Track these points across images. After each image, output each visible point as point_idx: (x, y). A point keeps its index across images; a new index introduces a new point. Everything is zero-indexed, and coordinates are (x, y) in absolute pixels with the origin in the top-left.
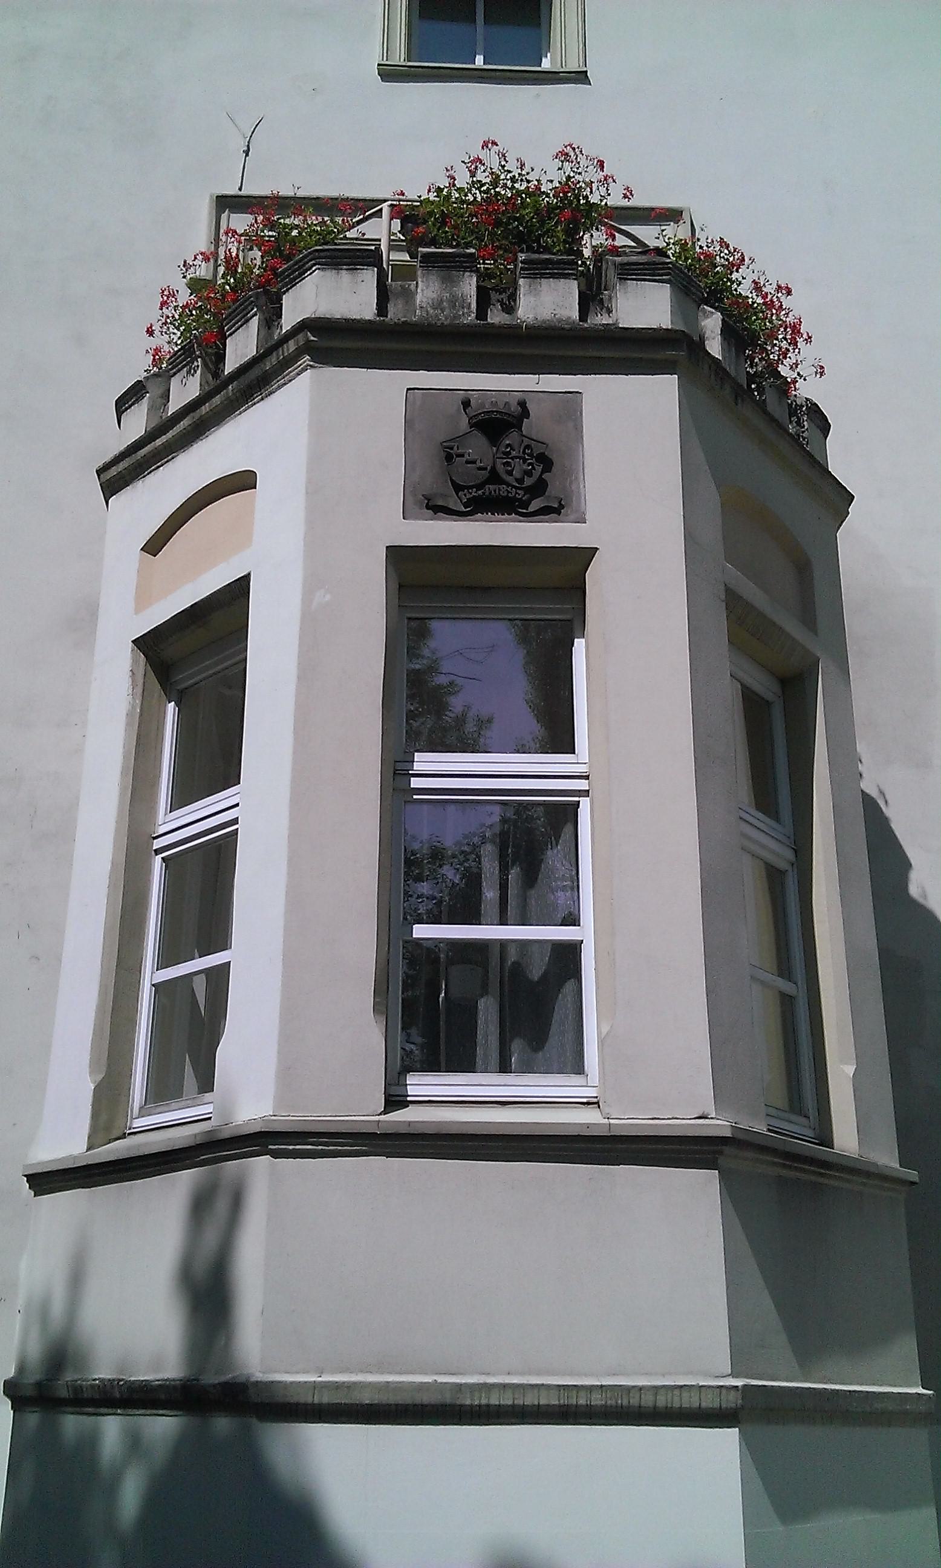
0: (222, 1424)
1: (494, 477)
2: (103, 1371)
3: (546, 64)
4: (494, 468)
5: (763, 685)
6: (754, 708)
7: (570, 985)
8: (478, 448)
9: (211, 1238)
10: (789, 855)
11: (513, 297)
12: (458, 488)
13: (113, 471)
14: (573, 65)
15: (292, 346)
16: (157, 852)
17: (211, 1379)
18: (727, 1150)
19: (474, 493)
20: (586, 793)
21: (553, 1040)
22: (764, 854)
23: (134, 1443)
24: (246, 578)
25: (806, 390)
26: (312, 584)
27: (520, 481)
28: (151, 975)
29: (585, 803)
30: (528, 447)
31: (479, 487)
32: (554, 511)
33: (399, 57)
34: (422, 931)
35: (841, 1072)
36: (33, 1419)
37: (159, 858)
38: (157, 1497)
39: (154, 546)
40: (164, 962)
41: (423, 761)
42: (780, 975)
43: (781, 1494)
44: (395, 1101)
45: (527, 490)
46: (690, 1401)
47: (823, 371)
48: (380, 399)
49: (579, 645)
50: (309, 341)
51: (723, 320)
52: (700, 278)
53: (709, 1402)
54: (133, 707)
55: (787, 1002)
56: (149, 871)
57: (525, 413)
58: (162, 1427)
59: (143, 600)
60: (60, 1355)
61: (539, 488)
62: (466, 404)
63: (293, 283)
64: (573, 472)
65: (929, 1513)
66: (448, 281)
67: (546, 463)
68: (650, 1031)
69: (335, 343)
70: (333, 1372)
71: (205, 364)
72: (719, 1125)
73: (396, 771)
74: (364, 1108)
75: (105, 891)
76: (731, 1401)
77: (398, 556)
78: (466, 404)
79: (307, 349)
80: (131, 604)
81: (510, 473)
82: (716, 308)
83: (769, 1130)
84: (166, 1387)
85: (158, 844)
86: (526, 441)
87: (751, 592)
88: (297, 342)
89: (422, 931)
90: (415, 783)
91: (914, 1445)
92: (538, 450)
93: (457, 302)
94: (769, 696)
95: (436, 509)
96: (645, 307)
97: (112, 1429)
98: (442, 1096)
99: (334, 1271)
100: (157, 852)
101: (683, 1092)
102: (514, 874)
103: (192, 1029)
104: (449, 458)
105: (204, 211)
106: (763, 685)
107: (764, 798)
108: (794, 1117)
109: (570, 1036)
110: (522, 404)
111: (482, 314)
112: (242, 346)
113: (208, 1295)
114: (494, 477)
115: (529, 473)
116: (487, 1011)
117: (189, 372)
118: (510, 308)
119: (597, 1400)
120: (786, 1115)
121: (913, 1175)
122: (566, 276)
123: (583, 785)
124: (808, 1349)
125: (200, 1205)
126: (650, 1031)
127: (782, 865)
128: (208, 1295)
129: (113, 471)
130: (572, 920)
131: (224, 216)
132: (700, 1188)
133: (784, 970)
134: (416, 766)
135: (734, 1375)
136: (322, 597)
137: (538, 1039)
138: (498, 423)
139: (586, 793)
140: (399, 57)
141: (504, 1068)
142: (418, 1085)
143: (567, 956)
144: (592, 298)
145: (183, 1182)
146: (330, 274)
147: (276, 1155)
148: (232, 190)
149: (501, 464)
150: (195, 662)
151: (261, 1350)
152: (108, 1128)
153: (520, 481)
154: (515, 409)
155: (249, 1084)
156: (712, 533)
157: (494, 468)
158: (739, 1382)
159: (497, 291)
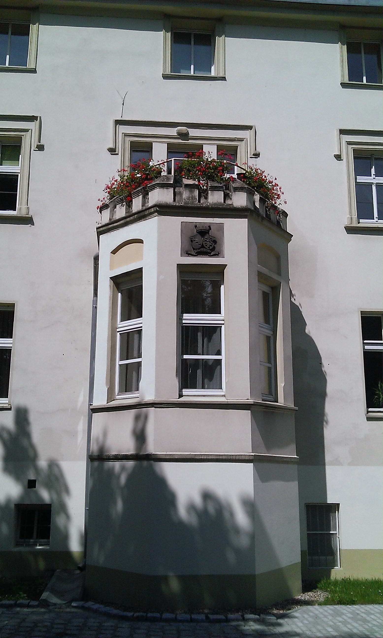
0: (145, 463)
1: (203, 246)
2: (114, 453)
3: (213, 74)
4: (203, 244)
5: (267, 289)
6: (265, 295)
7: (219, 367)
8: (199, 239)
9: (140, 425)
10: (272, 333)
11: (207, 194)
12: (194, 249)
13: (101, 229)
14: (221, 75)
15: (152, 210)
16: (118, 332)
17: (142, 453)
18: (253, 406)
19: (198, 250)
20: (224, 324)
21: (214, 379)
22: (265, 334)
23: (123, 468)
24: (142, 268)
25: (282, 207)
26: (159, 273)
27: (209, 248)
28: (118, 362)
29: (223, 326)
30: (211, 239)
31: (199, 249)
32: (217, 255)
33: (168, 72)
34: (185, 357)
35: (281, 385)
36: (96, 463)
37: (118, 333)
38: (130, 478)
39: (114, 252)
40: (121, 360)
41: (186, 316)
42: (268, 363)
43: (261, 477)
44: (181, 396)
45: (210, 250)
46: (243, 458)
47: (288, 201)
48: (175, 223)
49: (222, 286)
50: (157, 210)
51: (260, 197)
52: (255, 184)
53: (247, 458)
54: (111, 295)
55: (269, 369)
56: (116, 336)
57: (210, 229)
58: (130, 464)
59: (112, 267)
60: (102, 450)
61: (214, 249)
62: (196, 226)
63: (152, 190)
64: (222, 245)
65: (296, 483)
66: (191, 192)
67: (215, 242)
68: (237, 378)
69: (163, 210)
70: (169, 452)
71: (126, 203)
72: (251, 401)
73: (180, 319)
74: (175, 399)
75: (107, 342)
76: (252, 458)
77: (179, 266)
78: (196, 226)
79: (156, 211)
80: (109, 267)
81: (206, 245)
82: (258, 193)
83: (263, 400)
84: (131, 455)
85: (118, 330)
86: (211, 237)
87: (265, 271)
88: (154, 209)
89: (185, 357)
90: (184, 322)
91: (294, 468)
92: (213, 239)
93: (193, 198)
94: (269, 292)
95: (189, 254)
96: (240, 200)
97: (117, 465)
98: (192, 394)
99: (165, 432)
100: (118, 332)
101: (244, 395)
102: (205, 340)
103: (130, 377)
104: (192, 241)
105: (111, 124)
106: (267, 289)
107: (267, 321)
108: (270, 396)
109: (218, 379)
110: (210, 227)
111: (199, 201)
112: (137, 204)
113: (140, 437)
114: (203, 246)
115: (211, 246)
116: (199, 372)
117: (122, 205)
118: (206, 198)
119: (224, 457)
120: (269, 396)
121: (297, 408)
122: (220, 190)
123: (223, 322)
124: (269, 446)
125: (137, 418)
126: (237, 378)
127: (270, 335)
128: (140, 437)
129: (101, 229)
130: (219, 353)
131: (117, 126)
132: (247, 414)
133: (269, 362)
134: (184, 317)
135: (252, 453)
136: (162, 277)
137: (211, 379)
138: (204, 232)
139: (224, 324)
140: (168, 72)
141: (203, 388)
142: (185, 392)
143: (219, 362)
144: (226, 196)
145: (133, 412)
146: (161, 189)
147: (155, 407)
148: (119, 118)
149: (204, 242)
150: (129, 288)
151: (152, 448)
152: (111, 398)
153: (209, 248)
154: (208, 228)
155: (147, 390)
156: (255, 259)
157: (203, 244)
158: (253, 454)
159: (203, 193)
